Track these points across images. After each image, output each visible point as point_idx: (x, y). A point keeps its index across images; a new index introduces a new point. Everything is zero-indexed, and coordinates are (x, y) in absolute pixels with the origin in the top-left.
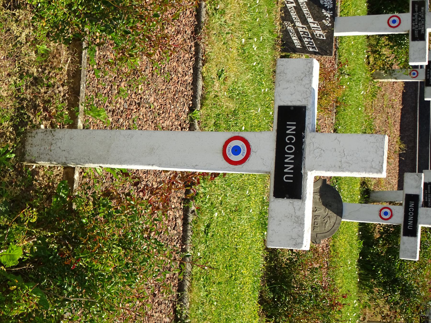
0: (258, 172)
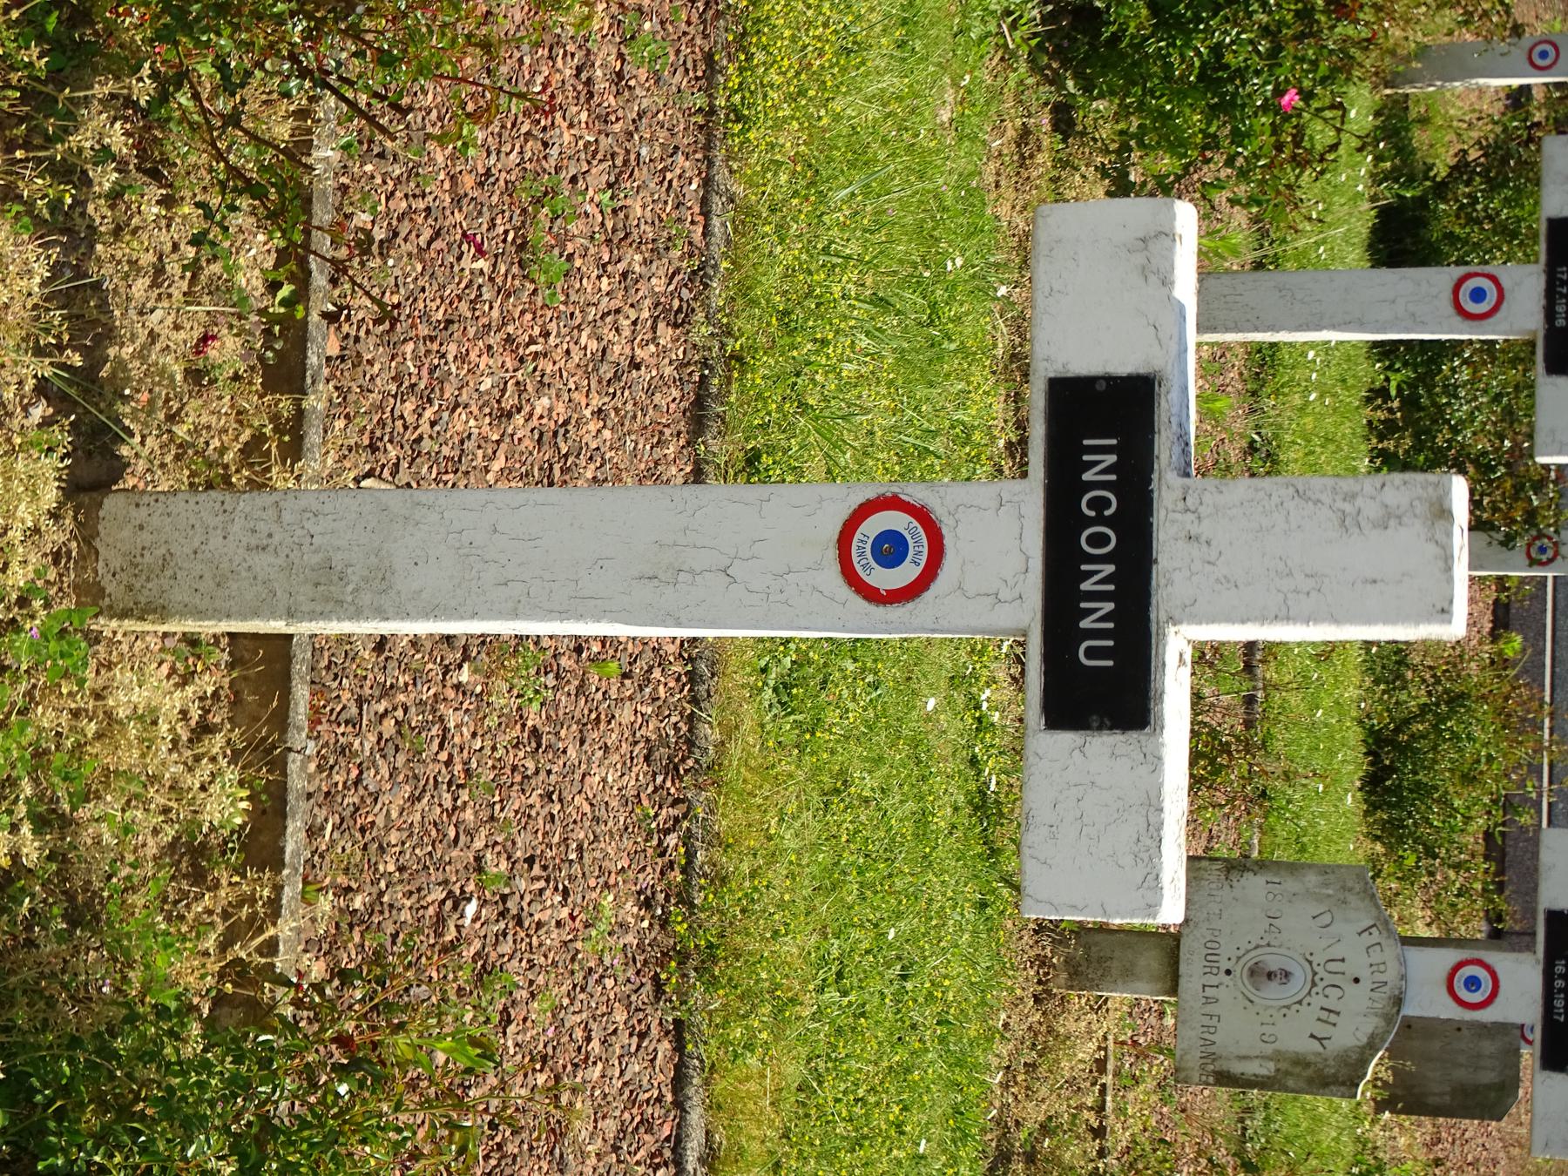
0: (983, 632)
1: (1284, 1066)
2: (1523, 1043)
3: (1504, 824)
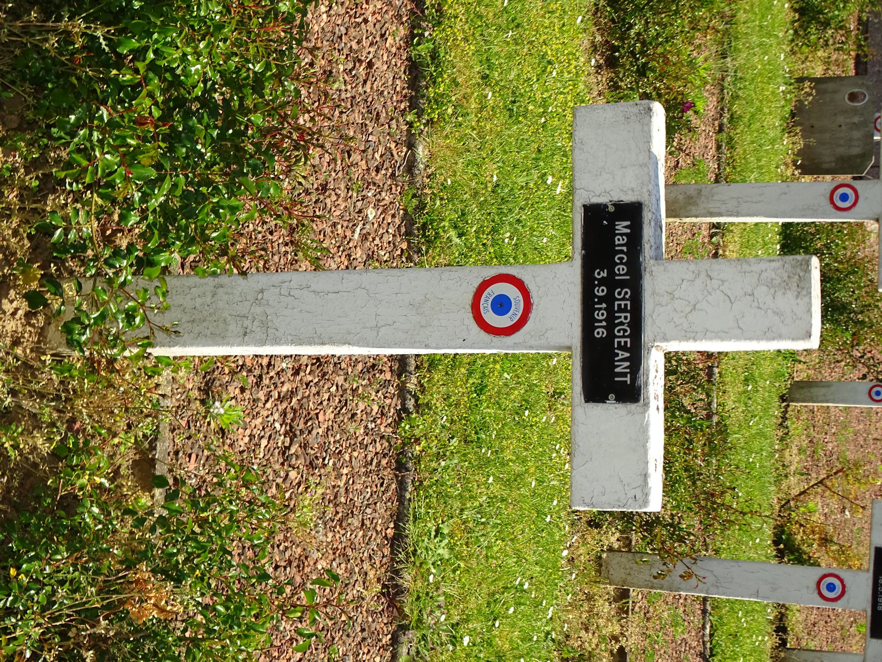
2: (875, 132)
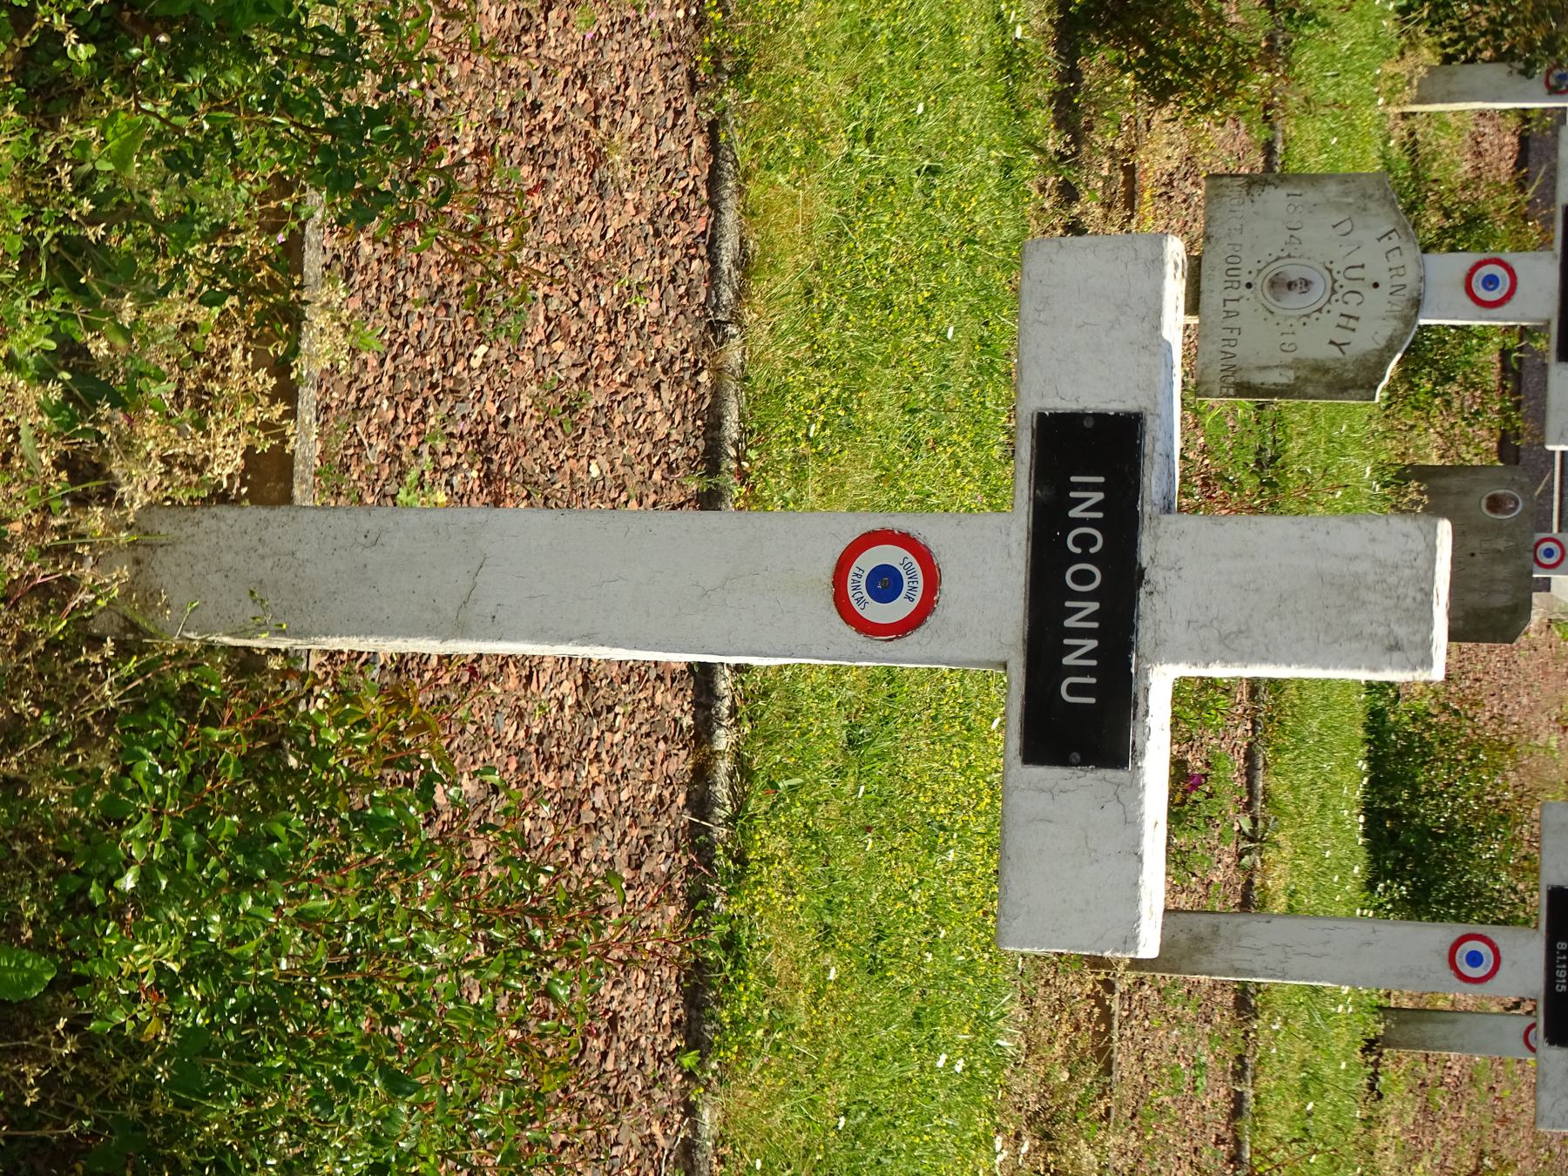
1: (1303, 373)
3: (1520, 350)
